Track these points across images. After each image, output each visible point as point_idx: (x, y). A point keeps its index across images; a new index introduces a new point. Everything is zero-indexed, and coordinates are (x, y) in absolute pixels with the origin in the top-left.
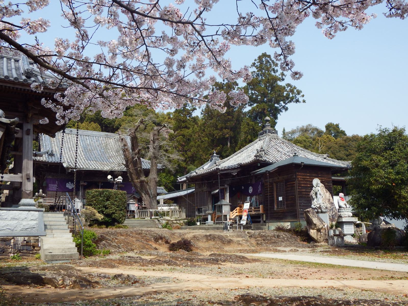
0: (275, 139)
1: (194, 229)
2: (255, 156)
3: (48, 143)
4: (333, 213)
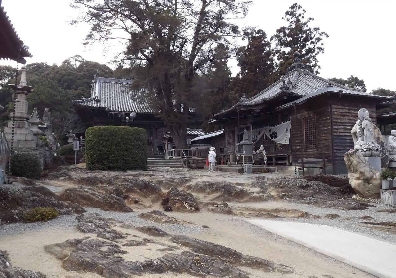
0: (305, 75)
1: (261, 214)
2: (280, 88)
3: (394, 215)
4: (383, 156)
